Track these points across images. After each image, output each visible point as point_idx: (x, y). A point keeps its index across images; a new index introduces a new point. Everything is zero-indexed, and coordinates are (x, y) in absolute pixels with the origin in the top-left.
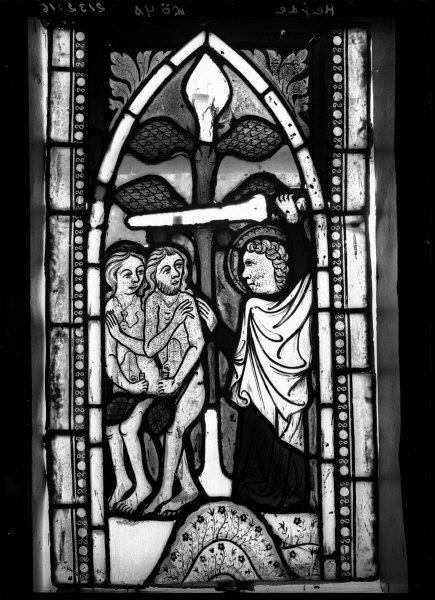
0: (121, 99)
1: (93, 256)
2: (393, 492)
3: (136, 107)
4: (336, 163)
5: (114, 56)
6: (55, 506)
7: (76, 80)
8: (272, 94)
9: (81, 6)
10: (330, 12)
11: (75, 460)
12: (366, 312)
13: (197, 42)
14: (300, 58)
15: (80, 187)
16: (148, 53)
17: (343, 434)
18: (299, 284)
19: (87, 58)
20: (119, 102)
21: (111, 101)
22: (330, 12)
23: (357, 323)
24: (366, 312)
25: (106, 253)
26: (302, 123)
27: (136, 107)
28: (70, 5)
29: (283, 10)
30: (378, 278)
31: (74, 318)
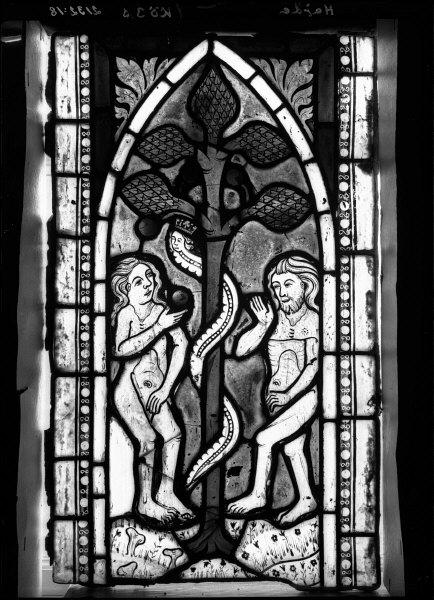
0: (126, 106)
1: (100, 272)
2: (391, 368)
3: (136, 125)
4: (86, 109)
5: (121, 63)
6: (57, 372)
7: (82, 210)
8: (274, 107)
9: (80, 8)
10: (330, 12)
11: (79, 332)
12: (372, 353)
13: (198, 53)
14: (302, 71)
15: (86, 357)
16: (153, 61)
17: (85, 337)
18: (301, 259)
19: (91, 163)
20: (124, 110)
21: (117, 110)
22: (330, 12)
23: (364, 365)
24: (372, 353)
25: (113, 263)
26: (306, 127)
27: (136, 125)
28: (72, 9)
29: (287, 11)
30: (382, 277)
31: (81, 367)
